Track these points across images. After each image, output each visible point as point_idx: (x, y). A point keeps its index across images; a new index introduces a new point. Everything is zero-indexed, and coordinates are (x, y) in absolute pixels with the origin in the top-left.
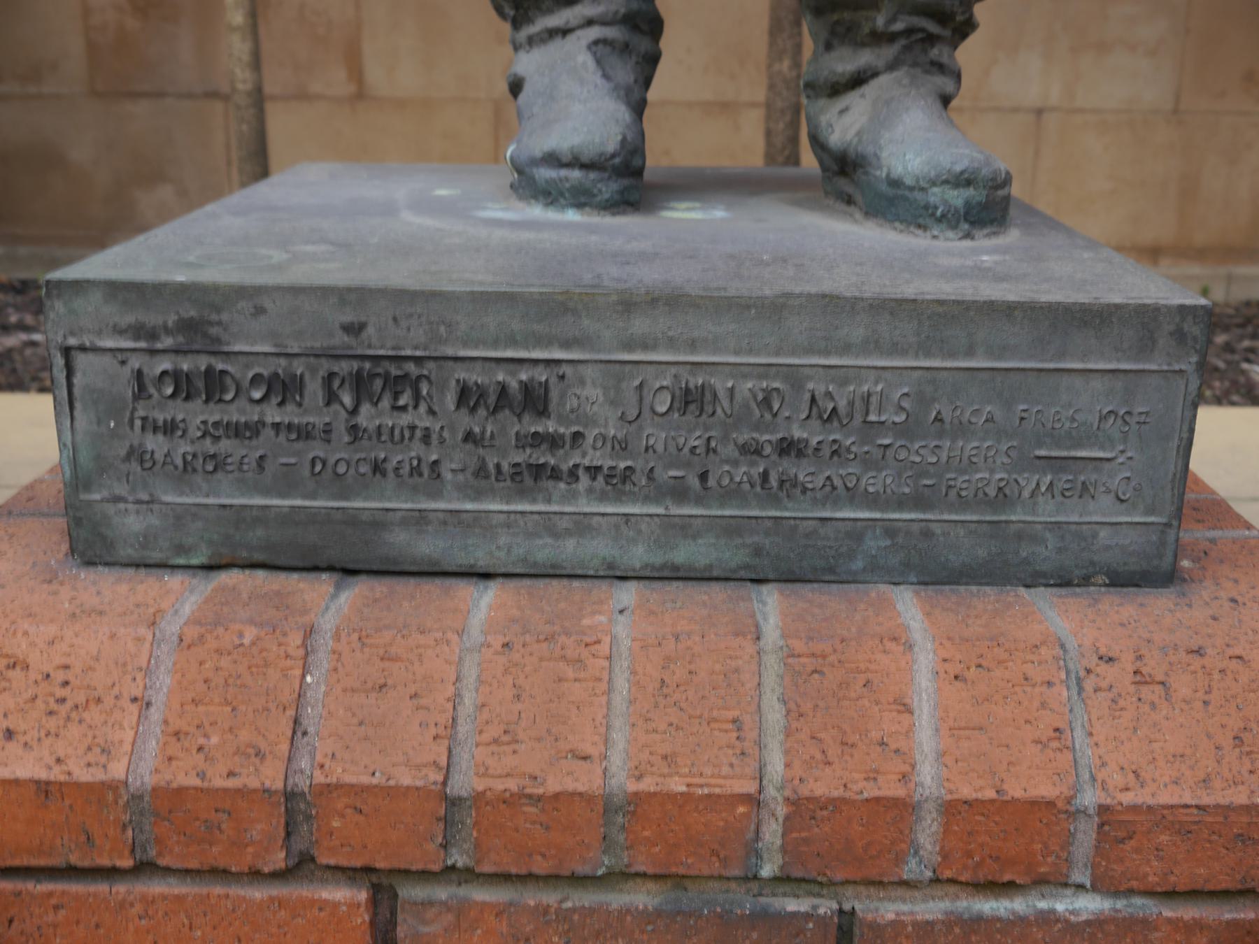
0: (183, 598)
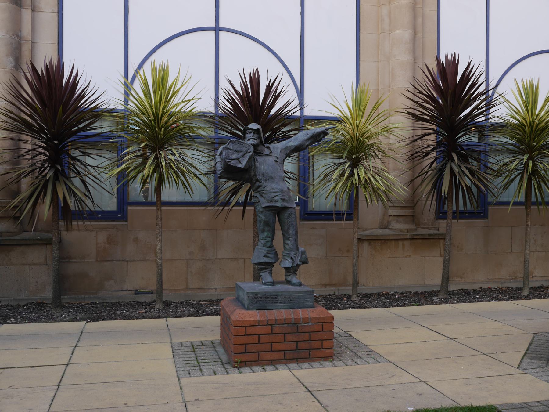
0: (257, 311)
